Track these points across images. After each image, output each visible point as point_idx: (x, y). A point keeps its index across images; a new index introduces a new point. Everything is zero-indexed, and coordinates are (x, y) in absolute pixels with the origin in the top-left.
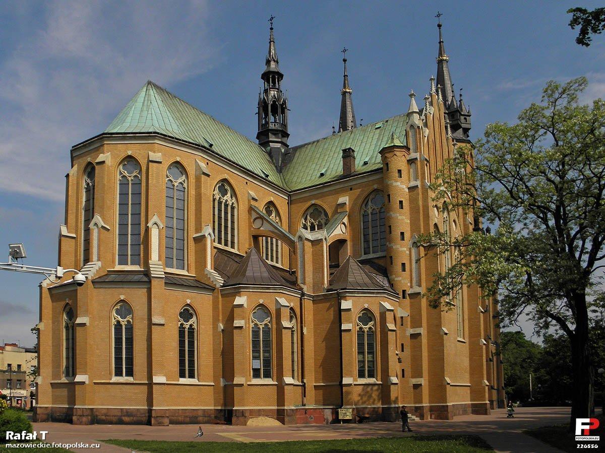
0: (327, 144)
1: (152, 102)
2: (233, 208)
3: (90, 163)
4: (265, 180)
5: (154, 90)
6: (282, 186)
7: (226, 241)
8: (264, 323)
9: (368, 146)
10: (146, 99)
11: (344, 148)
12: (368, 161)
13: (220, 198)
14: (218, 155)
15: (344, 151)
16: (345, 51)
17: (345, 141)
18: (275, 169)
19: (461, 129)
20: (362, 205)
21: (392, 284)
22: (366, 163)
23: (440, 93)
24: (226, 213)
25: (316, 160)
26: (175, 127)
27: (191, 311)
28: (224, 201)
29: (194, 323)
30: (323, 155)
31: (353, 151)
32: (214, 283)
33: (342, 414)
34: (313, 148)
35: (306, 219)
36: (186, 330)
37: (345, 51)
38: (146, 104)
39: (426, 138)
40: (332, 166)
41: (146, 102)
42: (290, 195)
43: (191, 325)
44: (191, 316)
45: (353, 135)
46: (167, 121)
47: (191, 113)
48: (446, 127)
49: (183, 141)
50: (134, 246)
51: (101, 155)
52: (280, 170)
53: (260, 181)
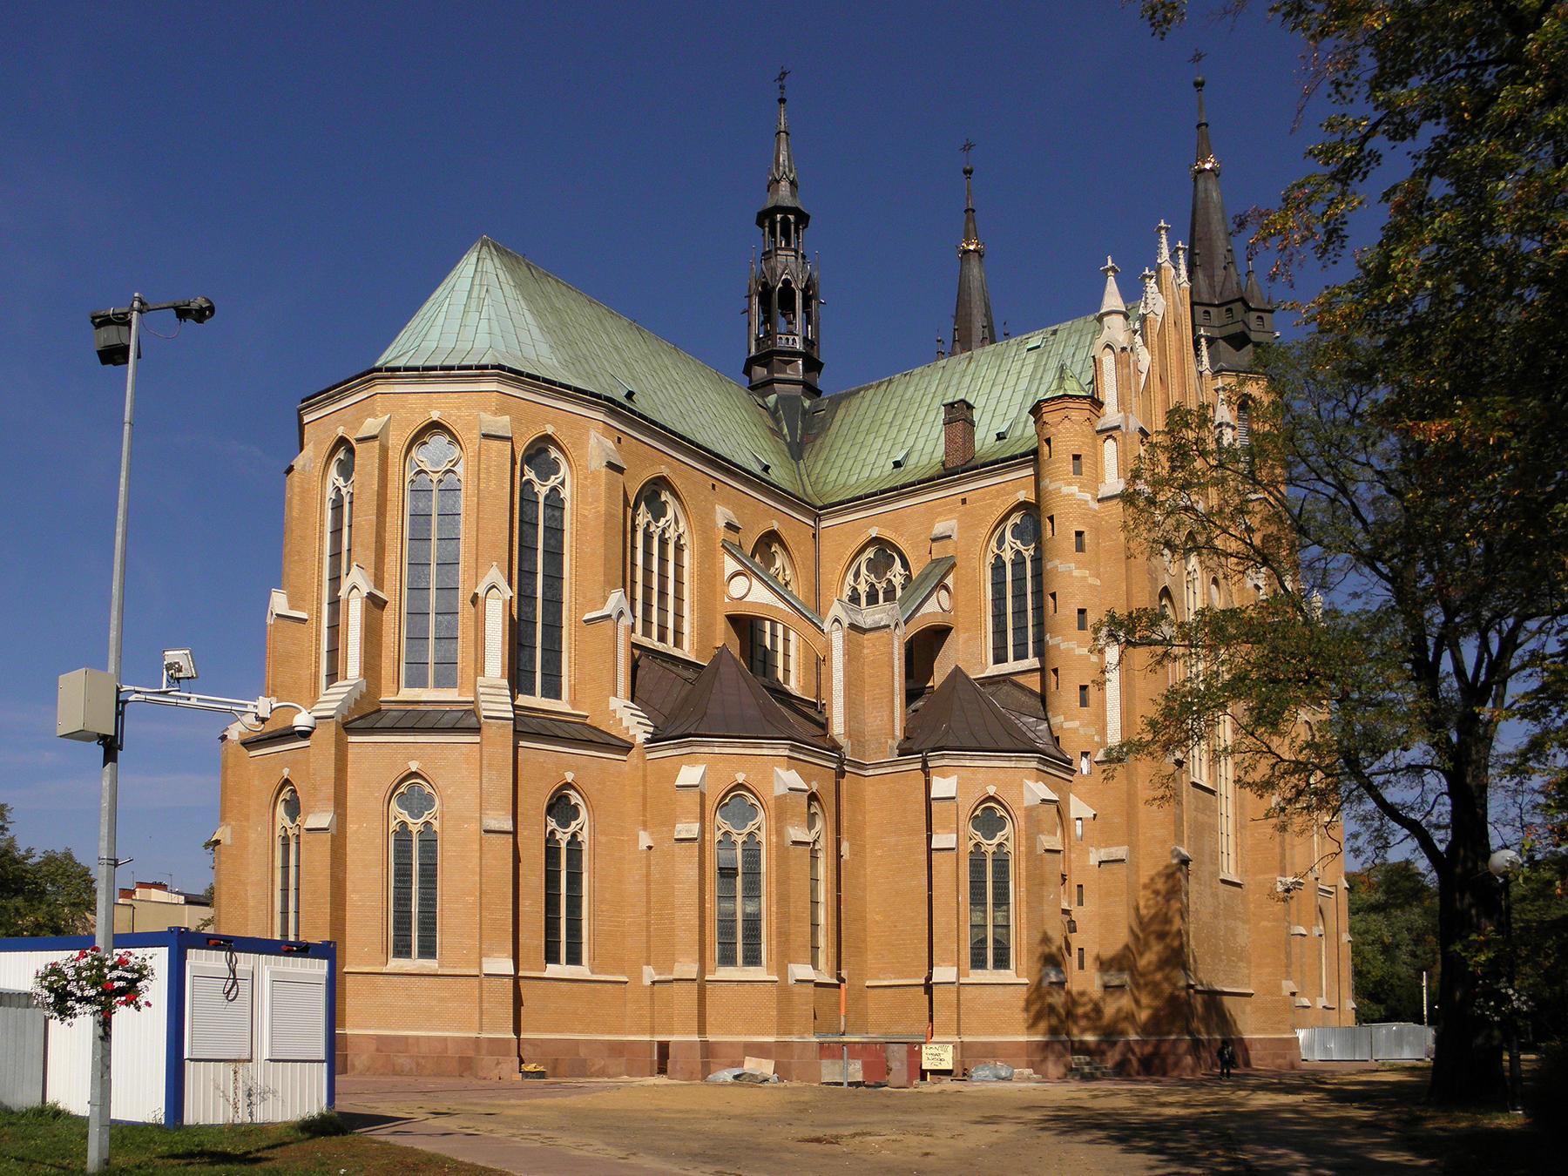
0: (912, 389)
1: (490, 288)
2: (679, 548)
3: (342, 441)
4: (759, 482)
5: (496, 260)
6: (800, 494)
7: (663, 628)
8: (746, 831)
9: (1007, 393)
10: (477, 282)
11: (950, 401)
12: (1007, 431)
13: (648, 524)
14: (645, 418)
15: (950, 407)
16: (967, 147)
17: (954, 382)
18: (786, 449)
19: (1250, 346)
20: (989, 541)
21: (1057, 738)
22: (1000, 437)
23: (1182, 261)
24: (663, 560)
25: (885, 428)
26: (544, 350)
27: (1001, 812)
28: (659, 531)
29: (1007, 839)
30: (900, 416)
31: (970, 407)
32: (631, 733)
33: (930, 1057)
34: (878, 399)
35: (857, 575)
36: (563, 845)
37: (967, 147)
38: (475, 294)
39: (1143, 377)
40: (920, 445)
41: (476, 288)
42: (818, 515)
43: (574, 835)
44: (1000, 824)
45: (973, 365)
46: (525, 337)
47: (582, 313)
48: (1196, 344)
49: (562, 385)
50: (412, 641)
51: (370, 420)
52: (797, 452)
53: (747, 482)
